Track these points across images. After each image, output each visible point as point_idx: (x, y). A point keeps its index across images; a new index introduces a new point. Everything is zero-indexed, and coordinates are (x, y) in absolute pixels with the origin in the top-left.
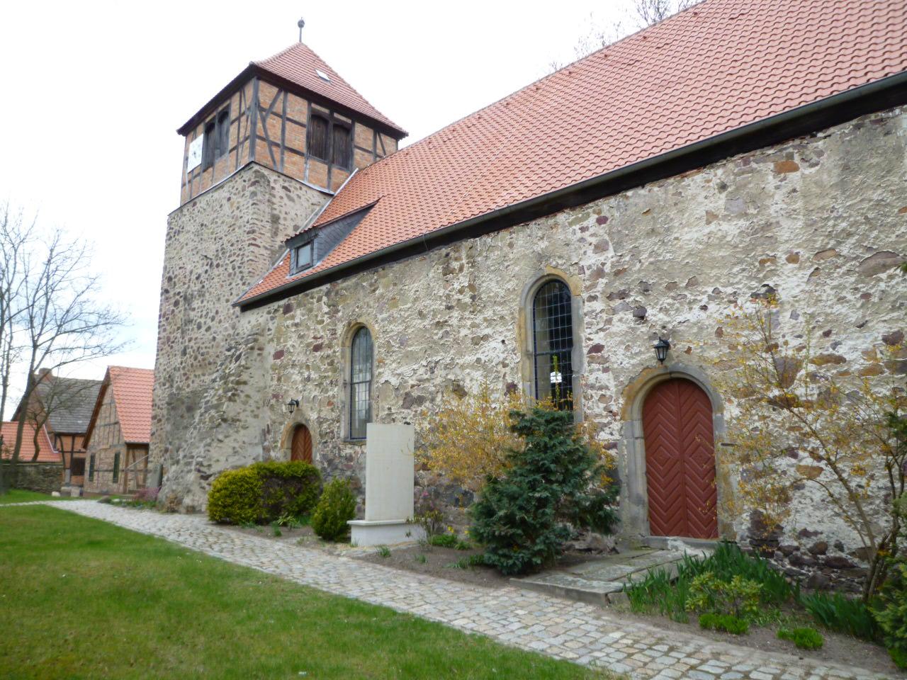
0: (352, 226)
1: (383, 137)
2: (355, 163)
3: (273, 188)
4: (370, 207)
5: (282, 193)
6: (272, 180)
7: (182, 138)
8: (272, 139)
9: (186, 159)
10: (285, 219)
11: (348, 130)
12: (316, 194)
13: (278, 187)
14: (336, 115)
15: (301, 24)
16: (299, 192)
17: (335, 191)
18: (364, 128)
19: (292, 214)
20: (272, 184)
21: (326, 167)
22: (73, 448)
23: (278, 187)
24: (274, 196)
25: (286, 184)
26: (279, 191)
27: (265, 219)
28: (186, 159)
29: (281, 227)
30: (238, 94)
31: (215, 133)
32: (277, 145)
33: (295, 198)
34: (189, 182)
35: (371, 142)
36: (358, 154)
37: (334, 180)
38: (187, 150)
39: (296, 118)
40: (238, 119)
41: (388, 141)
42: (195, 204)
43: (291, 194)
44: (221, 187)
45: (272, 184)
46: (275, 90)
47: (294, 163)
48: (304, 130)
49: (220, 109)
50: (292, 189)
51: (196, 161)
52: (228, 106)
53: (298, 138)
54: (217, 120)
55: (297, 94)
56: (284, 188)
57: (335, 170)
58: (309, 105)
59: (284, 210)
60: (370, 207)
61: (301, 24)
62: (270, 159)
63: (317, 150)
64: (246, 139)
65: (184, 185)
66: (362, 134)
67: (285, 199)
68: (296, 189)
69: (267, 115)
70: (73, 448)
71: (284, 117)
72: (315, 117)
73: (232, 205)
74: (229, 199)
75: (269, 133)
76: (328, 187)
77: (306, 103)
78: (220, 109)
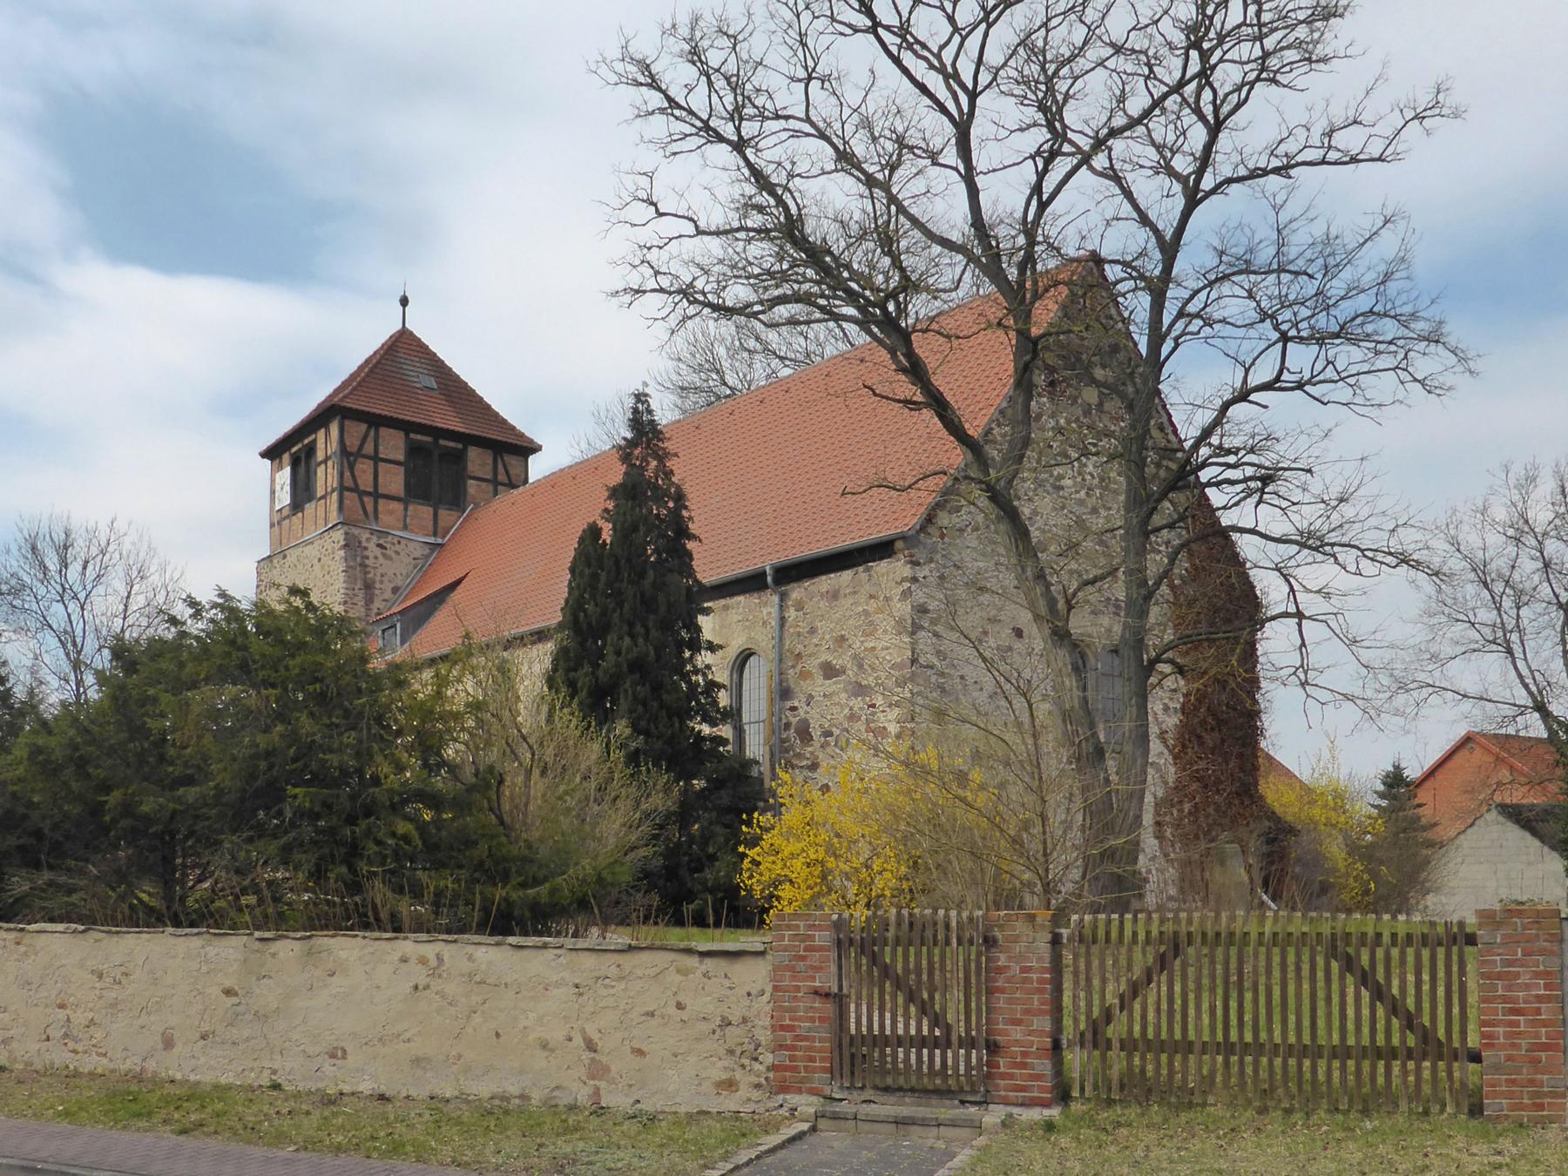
0: (442, 601)
1: (507, 458)
2: (469, 498)
3: (366, 548)
4: (458, 582)
5: (378, 551)
6: (363, 540)
7: (267, 462)
8: (362, 488)
9: (273, 492)
10: (381, 582)
11: (459, 458)
12: (417, 546)
13: (372, 546)
14: (442, 442)
15: (404, 302)
16: (397, 547)
17: (444, 537)
18: (480, 450)
19: (390, 573)
20: (364, 544)
21: (431, 510)
22: (1286, 615)
23: (372, 546)
24: (367, 558)
25: (381, 542)
26: (373, 550)
27: (357, 587)
28: (273, 492)
29: (377, 592)
30: (323, 430)
31: (302, 469)
32: (369, 494)
33: (393, 555)
34: (279, 523)
35: (489, 467)
36: (472, 487)
37: (441, 523)
38: (273, 481)
39: (391, 457)
40: (325, 461)
41: (512, 461)
42: (285, 557)
43: (388, 552)
44: (309, 543)
45: (364, 544)
46: (364, 427)
47: (391, 513)
48: (402, 469)
49: (306, 441)
50: (388, 546)
51: (285, 498)
52: (315, 441)
53: (394, 480)
54: (303, 456)
55: (388, 426)
56: (379, 546)
57: (443, 513)
58: (407, 435)
59: (379, 571)
60: (458, 582)
61: (404, 302)
62: (361, 512)
63: (417, 491)
64: (333, 491)
65: (272, 525)
66: (477, 461)
67: (380, 557)
68: (393, 544)
69: (355, 460)
70: (1286, 615)
71: (376, 459)
72: (414, 450)
73: (323, 567)
74: (319, 560)
75: (359, 482)
76: (435, 534)
77: (401, 434)
78: (306, 441)
